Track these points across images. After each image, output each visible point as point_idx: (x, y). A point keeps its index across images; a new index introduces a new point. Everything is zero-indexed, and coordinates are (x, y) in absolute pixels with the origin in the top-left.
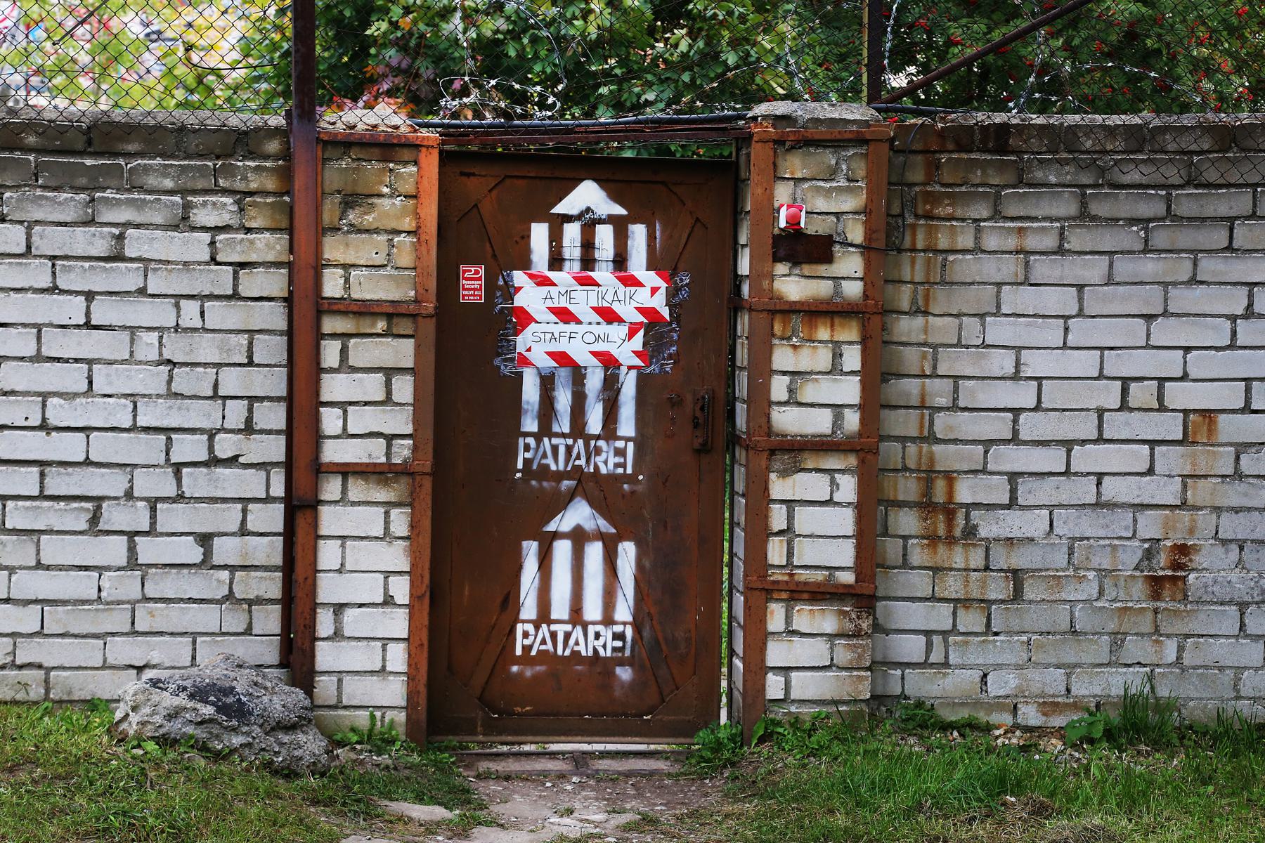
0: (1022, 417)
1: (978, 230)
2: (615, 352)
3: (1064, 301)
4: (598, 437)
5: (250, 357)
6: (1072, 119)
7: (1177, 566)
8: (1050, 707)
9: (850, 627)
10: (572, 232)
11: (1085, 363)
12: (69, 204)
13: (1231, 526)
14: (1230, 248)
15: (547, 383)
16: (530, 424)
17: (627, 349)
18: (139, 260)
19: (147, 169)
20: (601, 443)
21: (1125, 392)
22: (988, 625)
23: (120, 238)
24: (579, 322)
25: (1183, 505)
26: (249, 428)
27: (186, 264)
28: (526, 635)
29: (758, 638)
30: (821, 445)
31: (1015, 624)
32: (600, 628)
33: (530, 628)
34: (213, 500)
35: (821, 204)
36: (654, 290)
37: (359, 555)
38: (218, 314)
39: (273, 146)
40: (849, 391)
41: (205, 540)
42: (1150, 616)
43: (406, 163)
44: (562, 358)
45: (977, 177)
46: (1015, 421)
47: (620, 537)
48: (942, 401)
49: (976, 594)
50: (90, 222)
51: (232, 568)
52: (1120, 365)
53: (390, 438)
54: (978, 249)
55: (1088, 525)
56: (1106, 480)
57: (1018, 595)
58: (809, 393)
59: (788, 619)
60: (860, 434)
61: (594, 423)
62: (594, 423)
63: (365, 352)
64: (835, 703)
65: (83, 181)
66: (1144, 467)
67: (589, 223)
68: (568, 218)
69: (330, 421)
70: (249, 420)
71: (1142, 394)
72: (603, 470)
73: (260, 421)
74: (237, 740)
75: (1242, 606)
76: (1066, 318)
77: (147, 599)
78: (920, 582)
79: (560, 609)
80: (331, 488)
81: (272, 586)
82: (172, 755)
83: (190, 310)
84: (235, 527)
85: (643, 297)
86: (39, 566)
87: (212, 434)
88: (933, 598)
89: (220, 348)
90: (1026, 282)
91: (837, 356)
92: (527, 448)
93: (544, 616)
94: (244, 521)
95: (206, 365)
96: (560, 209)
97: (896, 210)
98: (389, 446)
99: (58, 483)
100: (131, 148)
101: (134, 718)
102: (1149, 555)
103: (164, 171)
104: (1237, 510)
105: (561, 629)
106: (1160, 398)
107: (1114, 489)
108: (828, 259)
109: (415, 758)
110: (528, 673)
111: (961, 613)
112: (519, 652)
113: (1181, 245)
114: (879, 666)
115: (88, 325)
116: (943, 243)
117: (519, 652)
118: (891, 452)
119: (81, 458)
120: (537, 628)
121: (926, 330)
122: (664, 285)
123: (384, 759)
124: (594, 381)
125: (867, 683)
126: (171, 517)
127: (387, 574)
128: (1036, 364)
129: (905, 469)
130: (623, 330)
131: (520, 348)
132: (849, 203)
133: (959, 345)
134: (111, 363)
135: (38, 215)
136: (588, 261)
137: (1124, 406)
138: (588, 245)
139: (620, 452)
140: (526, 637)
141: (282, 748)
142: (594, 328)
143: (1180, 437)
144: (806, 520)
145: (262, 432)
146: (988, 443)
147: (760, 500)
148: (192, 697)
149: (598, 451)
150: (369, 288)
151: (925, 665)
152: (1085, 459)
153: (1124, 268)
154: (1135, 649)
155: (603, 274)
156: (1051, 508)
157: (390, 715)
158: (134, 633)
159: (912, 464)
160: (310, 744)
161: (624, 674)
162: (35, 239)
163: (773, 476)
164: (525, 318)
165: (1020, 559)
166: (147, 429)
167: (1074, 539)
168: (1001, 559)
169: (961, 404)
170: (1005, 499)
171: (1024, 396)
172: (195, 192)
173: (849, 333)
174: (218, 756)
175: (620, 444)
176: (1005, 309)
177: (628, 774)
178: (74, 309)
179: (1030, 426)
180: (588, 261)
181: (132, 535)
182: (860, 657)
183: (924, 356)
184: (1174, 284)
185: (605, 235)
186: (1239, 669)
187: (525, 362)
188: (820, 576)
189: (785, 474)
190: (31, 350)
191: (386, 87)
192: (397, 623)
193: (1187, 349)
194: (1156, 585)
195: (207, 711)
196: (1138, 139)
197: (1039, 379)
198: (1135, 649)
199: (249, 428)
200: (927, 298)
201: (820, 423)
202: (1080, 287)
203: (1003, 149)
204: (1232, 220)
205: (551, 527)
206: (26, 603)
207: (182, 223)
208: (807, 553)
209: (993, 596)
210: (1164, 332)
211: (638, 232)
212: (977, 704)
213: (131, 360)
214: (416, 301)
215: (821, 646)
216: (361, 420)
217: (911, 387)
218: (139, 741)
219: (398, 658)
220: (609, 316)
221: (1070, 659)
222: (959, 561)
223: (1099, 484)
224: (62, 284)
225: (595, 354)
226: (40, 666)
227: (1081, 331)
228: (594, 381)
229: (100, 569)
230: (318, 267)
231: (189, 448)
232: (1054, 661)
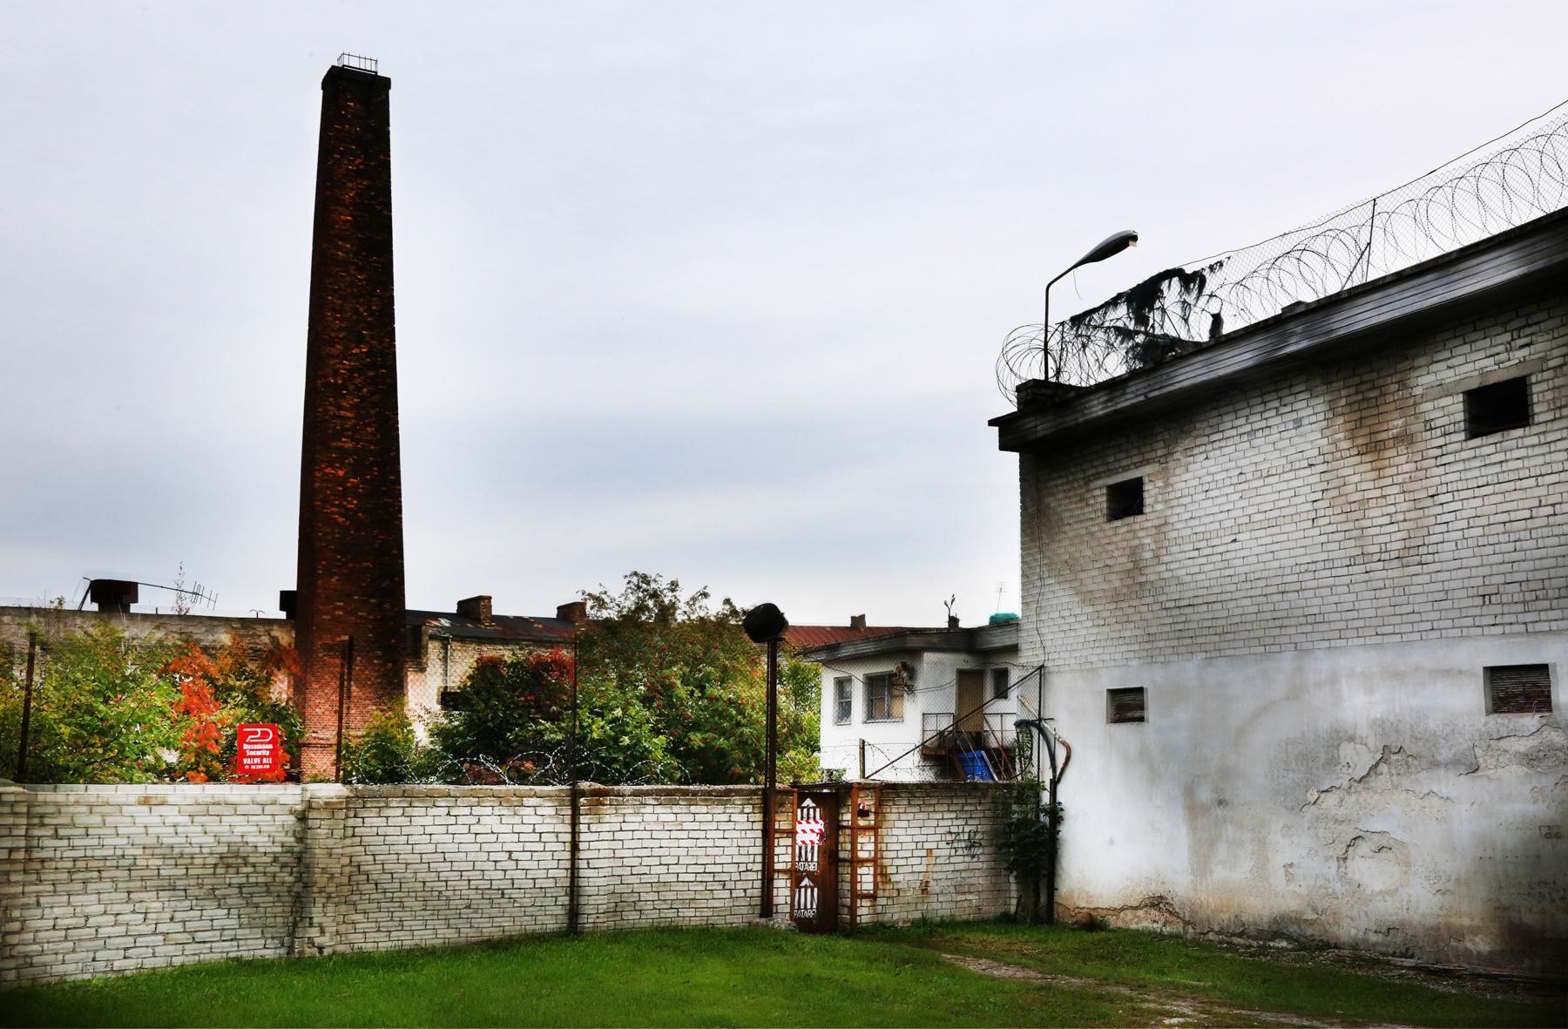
10: (805, 810)
12: (720, 809)
15: (800, 848)
17: (816, 838)
30: (867, 860)
40: (872, 847)
41: (745, 890)
44: (803, 842)
79: (802, 907)
93: (799, 908)
108: (868, 816)
132: (871, 803)
136: (808, 818)
138: (808, 814)
153: (917, 816)
155: (811, 821)
165: (900, 886)
178: (720, 834)
180: (808, 818)
198: (919, 906)
207: (742, 812)
211: (818, 810)
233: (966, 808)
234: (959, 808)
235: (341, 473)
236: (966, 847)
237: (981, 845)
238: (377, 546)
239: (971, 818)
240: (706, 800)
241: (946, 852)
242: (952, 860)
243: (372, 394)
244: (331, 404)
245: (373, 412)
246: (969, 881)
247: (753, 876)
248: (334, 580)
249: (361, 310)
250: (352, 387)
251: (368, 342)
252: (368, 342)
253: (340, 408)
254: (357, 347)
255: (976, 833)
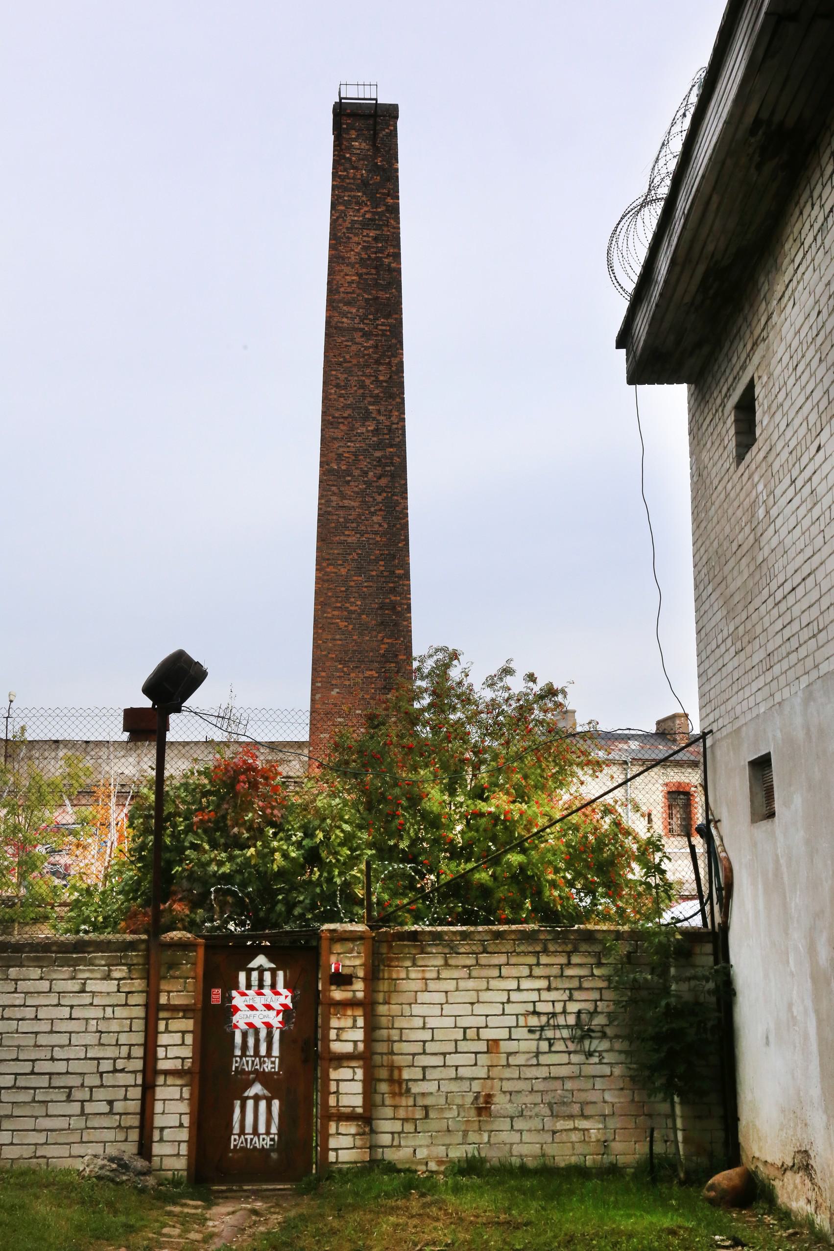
0: (427, 1044)
1: (408, 971)
2: (271, 1022)
3: (440, 998)
4: (264, 1057)
5: (131, 1028)
6: (439, 929)
7: (487, 1102)
8: (440, 1162)
9: (361, 1131)
10: (255, 975)
11: (450, 1022)
12: (66, 971)
13: (507, 1086)
14: (500, 976)
15: (245, 1035)
16: (238, 1052)
17: (276, 1020)
18: (91, 992)
19: (95, 957)
20: (266, 1059)
21: (465, 1033)
22: (416, 1129)
23: (84, 984)
24: (257, 1010)
25: (488, 1078)
26: (129, 1057)
27: (108, 993)
28: (235, 1140)
29: (326, 1136)
30: (349, 1057)
31: (426, 1128)
32: (264, 1136)
33: (237, 1137)
34: (114, 1086)
35: (347, 963)
36: (286, 997)
37: (172, 1107)
38: (120, 1012)
39: (143, 946)
40: (359, 1035)
41: (110, 1103)
42: (477, 1123)
43: (192, 952)
44: (250, 1025)
45: (406, 950)
46: (424, 1046)
47: (272, 1098)
48: (396, 1038)
49: (411, 1116)
50: (73, 978)
51: (121, 1114)
52: (463, 1022)
53: (183, 1059)
54: (408, 978)
55: (453, 1087)
56: (459, 1068)
57: (427, 1116)
58: (345, 1036)
59: (337, 1128)
60: (364, 1052)
61: (263, 1051)
62: (263, 1051)
63: (174, 1025)
64: (356, 1162)
65: (71, 963)
66: (473, 1063)
67: (261, 970)
68: (253, 969)
69: (161, 1053)
70: (129, 1054)
71: (471, 1034)
72: (267, 1070)
73: (133, 1054)
74: (125, 1178)
75: (512, 1118)
76: (442, 1004)
77: (87, 1128)
78: (388, 1112)
79: (249, 1129)
80: (160, 1080)
81: (135, 1121)
82: (102, 1183)
83: (109, 1010)
84: (122, 1097)
85: (282, 1000)
86: (47, 1116)
87: (115, 1060)
88: (394, 1119)
89: (120, 1026)
90: (426, 991)
91: (355, 1021)
92: (236, 1062)
93: (242, 1132)
94: (126, 1095)
95: (114, 1032)
96: (251, 966)
97: (376, 964)
98: (183, 1062)
99: (56, 1082)
100: (91, 949)
101: (88, 1170)
102: (476, 1098)
103: (102, 958)
104: (508, 1079)
105: (249, 1137)
106: (478, 1035)
107: (462, 1072)
108: (351, 983)
109: (191, 1190)
110: (236, 1157)
111: (405, 1124)
112: (232, 1147)
113: (482, 975)
114: (372, 1147)
115: (71, 1018)
116: (394, 976)
117: (232, 1147)
118: (377, 1059)
119: (65, 1071)
120: (240, 1137)
121: (389, 1010)
122: (290, 994)
123: (178, 1190)
124: (263, 1034)
125: (368, 1154)
126: (99, 1094)
127: (181, 1114)
128: (431, 1023)
129: (383, 1066)
130: (275, 1013)
131: (234, 1021)
132: (358, 962)
133: (402, 1016)
134: (78, 1033)
135: (55, 976)
136: (261, 986)
137: (465, 1039)
139: (273, 1063)
140: (235, 1141)
141: (140, 1183)
142: (263, 1013)
143: (486, 1050)
144: (344, 1087)
145: (134, 1058)
146: (414, 1055)
147: (327, 1080)
148: (109, 1161)
149: (264, 1062)
150: (177, 999)
151: (391, 1146)
152: (452, 1060)
153: (463, 984)
154: (473, 1137)
155: (267, 991)
156: (439, 1080)
157: (181, 1173)
158: (82, 1142)
159: (385, 1064)
160: (151, 1181)
161: (274, 1155)
162: (53, 986)
163: (331, 1070)
164: (237, 1009)
165: (428, 1101)
166: (91, 1059)
167: (448, 1093)
168: (420, 1102)
169: (404, 1039)
170: (421, 1077)
171: (426, 1035)
172: (113, 965)
173: (359, 1012)
174: (117, 1183)
175: (273, 1059)
176: (419, 1001)
177: (274, 1196)
178: (65, 1012)
179: (429, 1048)
180: (261, 986)
181: (83, 1102)
182: (365, 1143)
183: (389, 1020)
184: (481, 990)
185: (267, 976)
186: (512, 1144)
187: (236, 1027)
188: (349, 1110)
189: (336, 1069)
190: (48, 1029)
191: (180, 896)
192: (184, 1135)
193: (487, 1016)
194: (480, 1111)
195: (114, 1166)
196: (464, 935)
197: (433, 1029)
198: (473, 1137)
199: (129, 1057)
200: (389, 997)
201: (348, 1048)
202: (446, 992)
203: (415, 940)
204: (500, 966)
205: (246, 1094)
206: (41, 1131)
207: (108, 977)
208: (345, 1101)
209: (417, 1117)
210: (479, 1009)
211: (280, 974)
212: (412, 1162)
213: (86, 1032)
214: (195, 1004)
215: (350, 1139)
216: (173, 1052)
217: (384, 1033)
218: (90, 1177)
219: (184, 1149)
220: (269, 1007)
221: (447, 1142)
222: (404, 1103)
223: (456, 1070)
224: (62, 1003)
225: (264, 1023)
226: (45, 1157)
227: (448, 1010)
228: (263, 1034)
229: (70, 1116)
230: (158, 992)
231: (106, 1066)
232: (441, 1143)
233: (569, 972)
234: (555, 971)
235: (343, 571)
236: (572, 1039)
237: (604, 1035)
238: (382, 652)
239: (580, 988)
240: (37, 959)
241: (532, 1046)
242: (543, 1059)
243: (380, 477)
244: (334, 494)
245: (379, 498)
246: (583, 1097)
247: (128, 1079)
248: (334, 693)
249: (368, 382)
250: (356, 473)
251: (374, 419)
252: (374, 419)
253: (343, 497)
254: (363, 425)
255: (593, 1013)
